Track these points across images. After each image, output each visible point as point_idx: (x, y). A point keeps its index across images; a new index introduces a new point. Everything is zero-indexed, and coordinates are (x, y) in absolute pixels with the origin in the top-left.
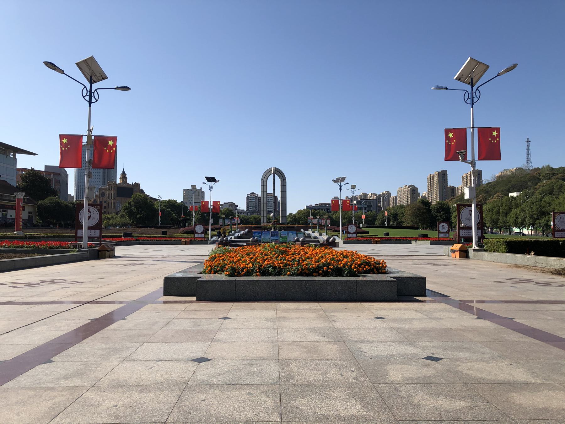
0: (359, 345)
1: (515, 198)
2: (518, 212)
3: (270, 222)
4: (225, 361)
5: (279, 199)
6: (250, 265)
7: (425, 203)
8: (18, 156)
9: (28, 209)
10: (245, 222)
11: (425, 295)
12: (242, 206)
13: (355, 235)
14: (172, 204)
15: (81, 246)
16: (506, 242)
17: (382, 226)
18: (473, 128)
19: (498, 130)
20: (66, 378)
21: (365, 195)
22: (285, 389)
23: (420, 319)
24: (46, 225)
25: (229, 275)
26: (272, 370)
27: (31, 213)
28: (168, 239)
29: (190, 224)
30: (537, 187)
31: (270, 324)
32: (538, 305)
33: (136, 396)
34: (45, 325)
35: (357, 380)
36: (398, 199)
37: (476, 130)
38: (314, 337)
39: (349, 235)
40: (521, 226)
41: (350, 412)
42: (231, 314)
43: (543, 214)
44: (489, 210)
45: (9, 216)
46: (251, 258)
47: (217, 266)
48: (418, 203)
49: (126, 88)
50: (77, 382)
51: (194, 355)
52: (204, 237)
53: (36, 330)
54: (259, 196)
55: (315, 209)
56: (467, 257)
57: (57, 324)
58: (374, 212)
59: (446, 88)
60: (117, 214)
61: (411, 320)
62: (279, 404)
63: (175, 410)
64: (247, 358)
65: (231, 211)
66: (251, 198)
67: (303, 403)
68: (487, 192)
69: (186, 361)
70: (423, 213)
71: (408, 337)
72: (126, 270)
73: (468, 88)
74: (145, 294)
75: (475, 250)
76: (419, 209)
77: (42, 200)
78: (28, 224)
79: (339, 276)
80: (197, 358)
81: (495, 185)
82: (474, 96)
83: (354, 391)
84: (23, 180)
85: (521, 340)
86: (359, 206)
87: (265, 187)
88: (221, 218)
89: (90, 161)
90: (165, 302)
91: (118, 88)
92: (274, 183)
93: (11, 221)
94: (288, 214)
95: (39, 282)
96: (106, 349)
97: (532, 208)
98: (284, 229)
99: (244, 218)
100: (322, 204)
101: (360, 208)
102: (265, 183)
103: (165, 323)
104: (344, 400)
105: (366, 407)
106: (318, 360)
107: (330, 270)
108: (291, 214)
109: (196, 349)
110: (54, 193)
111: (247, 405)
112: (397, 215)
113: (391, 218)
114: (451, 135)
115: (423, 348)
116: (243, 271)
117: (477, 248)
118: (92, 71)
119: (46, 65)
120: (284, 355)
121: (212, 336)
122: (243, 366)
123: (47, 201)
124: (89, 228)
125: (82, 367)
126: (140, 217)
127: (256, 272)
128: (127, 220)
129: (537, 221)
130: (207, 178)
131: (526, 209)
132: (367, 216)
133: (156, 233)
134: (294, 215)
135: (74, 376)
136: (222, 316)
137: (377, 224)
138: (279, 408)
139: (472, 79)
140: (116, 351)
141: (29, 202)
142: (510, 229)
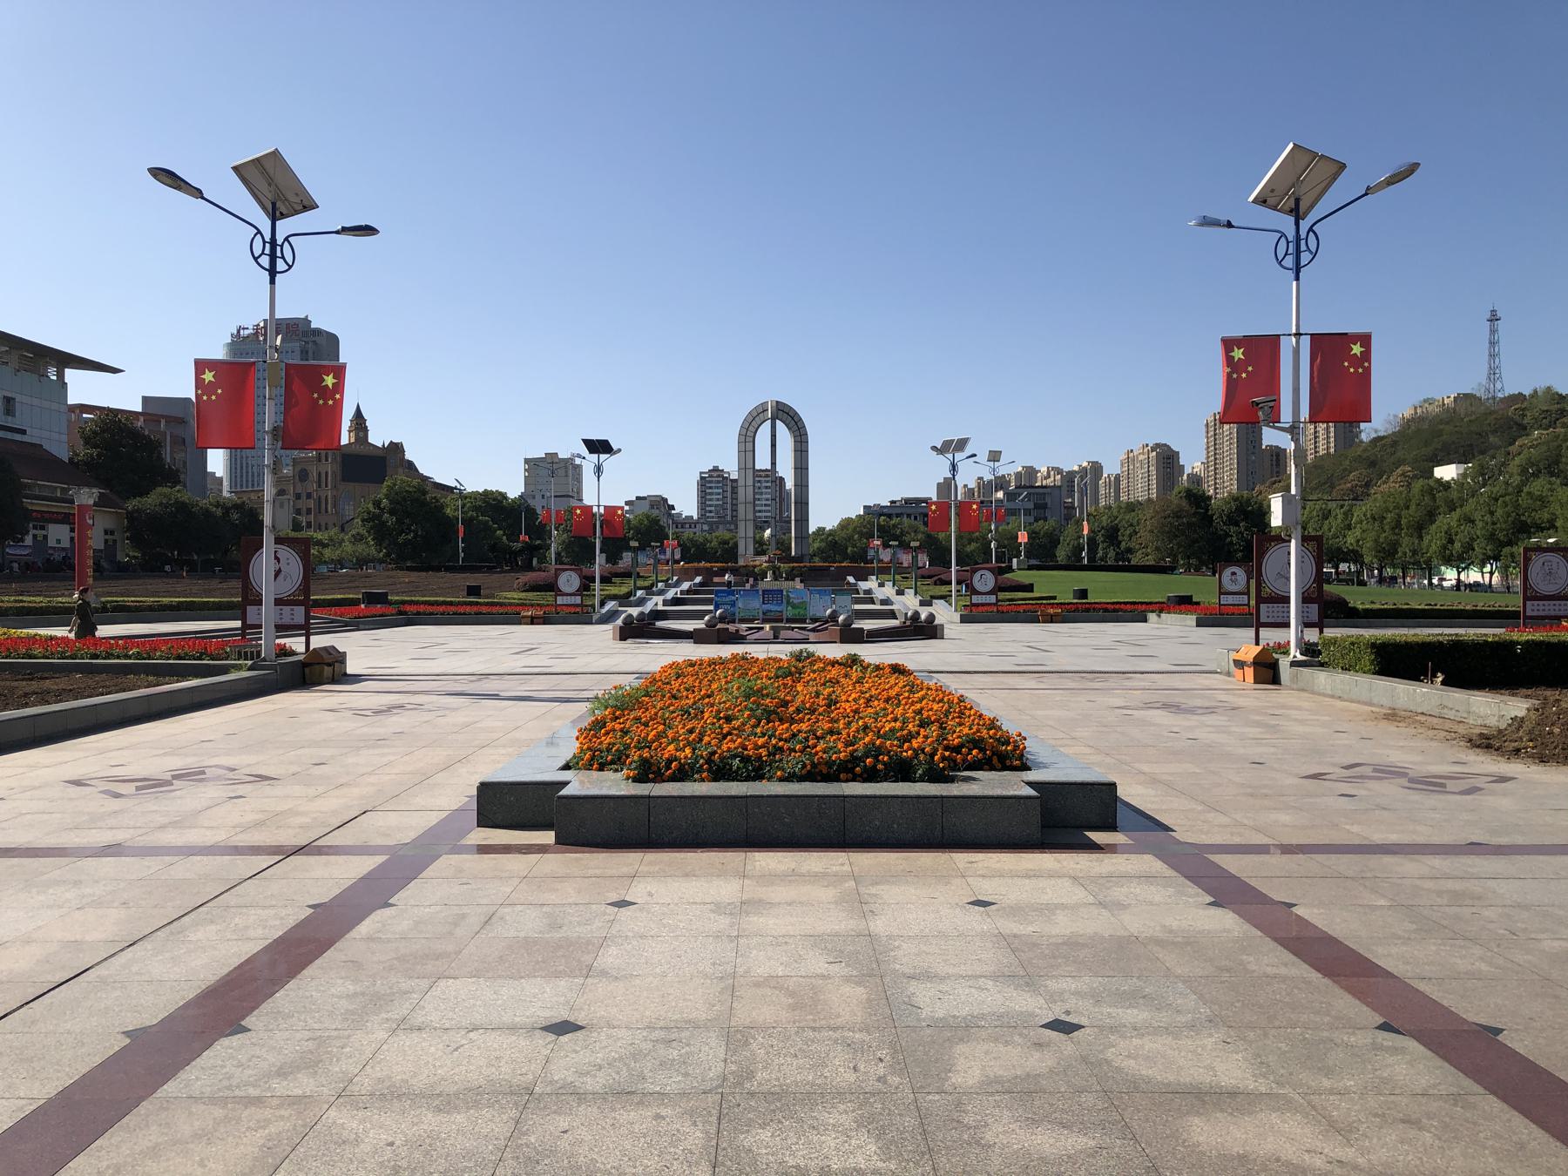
0: (913, 987)
1: (1444, 485)
3: (763, 553)
4: (613, 1032)
5: (790, 484)
7: (1196, 497)
8: (71, 375)
10: (694, 552)
11: (1111, 827)
12: (686, 505)
13: (992, 599)
14: (492, 503)
15: (259, 653)
16: (1373, 645)
17: (1074, 565)
18: (1298, 335)
19: (1365, 340)
20: (282, 1072)
21: (1031, 472)
22: (733, 1103)
23: (1074, 908)
24: (151, 567)
25: (637, 780)
26: (711, 1056)
27: (112, 533)
28: (484, 609)
29: (543, 559)
30: (1513, 449)
31: (723, 922)
35: (885, 1082)
36: (1123, 484)
37: (1306, 342)
38: (817, 963)
39: (976, 599)
40: (1460, 561)
41: (851, 1162)
42: (637, 892)
43: (1524, 528)
45: (52, 543)
46: (691, 731)
47: (609, 750)
48: (1174, 497)
49: (368, 230)
50: (303, 1084)
51: (547, 1014)
52: (582, 605)
53: (193, 937)
54: (734, 476)
55: (890, 516)
56: (1275, 680)
58: (1052, 522)
59: (1229, 225)
62: (714, 1143)
64: (662, 1024)
65: (655, 521)
66: (711, 482)
67: (761, 1140)
68: (1373, 464)
70: (1189, 525)
71: (1026, 962)
73: (1286, 223)
74: (433, 819)
75: (1294, 664)
76: (1177, 515)
77: (141, 495)
78: (109, 568)
80: (554, 1021)
81: (1394, 444)
82: (1303, 247)
83: (872, 1111)
84: (88, 441)
85: (1283, 971)
86: (1011, 505)
88: (629, 549)
90: (484, 849)
91: (345, 230)
92: (773, 445)
93: (58, 557)
94: (812, 529)
95: (168, 776)
96: (355, 994)
97: (1492, 513)
99: (691, 540)
100: (908, 501)
101: (1013, 512)
102: (749, 446)
103: (483, 919)
104: (846, 1133)
105: (885, 1153)
106: (814, 1029)
107: (880, 766)
108: (821, 530)
109: (547, 998)
110: (172, 477)
111: (650, 1145)
113: (1100, 538)
115: (1053, 998)
116: (668, 768)
117: (1300, 657)
118: (275, 187)
119: (155, 176)
120: (744, 1014)
121: (587, 959)
122: (650, 1046)
123: (152, 501)
124: (278, 602)
126: (407, 542)
127: (700, 771)
128: (370, 548)
129: (1506, 550)
130: (585, 441)
131: (1477, 516)
132: (1032, 535)
133: (447, 586)
134: (832, 533)
136: (614, 897)
137: (1061, 554)
138: (713, 1151)
139: (1297, 201)
140: (377, 1001)
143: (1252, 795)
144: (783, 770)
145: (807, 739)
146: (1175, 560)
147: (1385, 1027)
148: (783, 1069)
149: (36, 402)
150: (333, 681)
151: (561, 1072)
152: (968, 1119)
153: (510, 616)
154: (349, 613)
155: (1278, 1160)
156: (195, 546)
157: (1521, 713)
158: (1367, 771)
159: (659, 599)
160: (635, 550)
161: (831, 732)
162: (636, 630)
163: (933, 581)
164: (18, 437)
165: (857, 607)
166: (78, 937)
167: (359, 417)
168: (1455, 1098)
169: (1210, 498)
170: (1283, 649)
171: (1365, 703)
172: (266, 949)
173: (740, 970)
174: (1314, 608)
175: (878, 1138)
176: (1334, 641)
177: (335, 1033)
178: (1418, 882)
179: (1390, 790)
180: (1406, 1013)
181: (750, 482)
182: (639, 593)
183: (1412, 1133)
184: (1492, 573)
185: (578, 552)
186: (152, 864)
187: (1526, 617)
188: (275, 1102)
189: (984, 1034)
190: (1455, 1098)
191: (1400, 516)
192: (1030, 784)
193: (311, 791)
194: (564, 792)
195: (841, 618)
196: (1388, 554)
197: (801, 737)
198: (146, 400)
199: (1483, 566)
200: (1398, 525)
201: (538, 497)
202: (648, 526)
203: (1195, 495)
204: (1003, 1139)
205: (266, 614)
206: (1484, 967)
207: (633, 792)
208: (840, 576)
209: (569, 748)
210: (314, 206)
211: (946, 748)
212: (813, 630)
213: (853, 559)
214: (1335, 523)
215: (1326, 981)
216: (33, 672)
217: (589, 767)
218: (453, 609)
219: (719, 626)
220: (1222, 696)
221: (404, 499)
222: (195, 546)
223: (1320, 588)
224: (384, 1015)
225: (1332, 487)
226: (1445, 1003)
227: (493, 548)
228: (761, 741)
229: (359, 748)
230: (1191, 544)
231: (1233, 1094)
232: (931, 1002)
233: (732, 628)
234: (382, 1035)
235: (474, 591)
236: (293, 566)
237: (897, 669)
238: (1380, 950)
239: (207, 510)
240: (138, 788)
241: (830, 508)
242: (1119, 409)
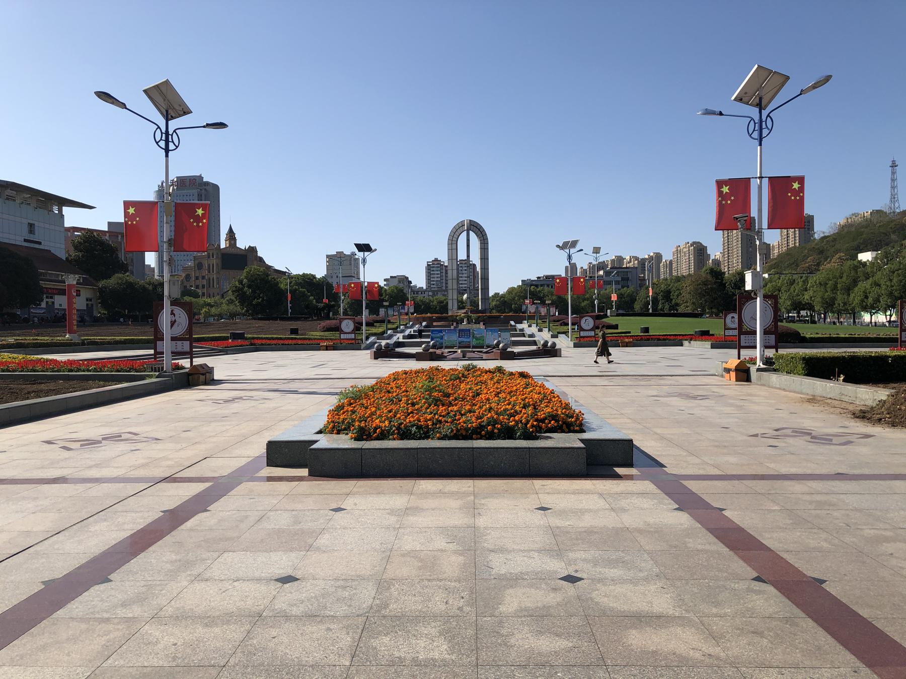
0: (492, 556)
1: (864, 264)
2: (868, 286)
3: (463, 308)
6: (387, 422)
7: (716, 273)
8: (66, 210)
9: (86, 293)
10: (422, 308)
11: (630, 465)
12: (419, 280)
14: (308, 281)
15: (163, 368)
16: (804, 359)
18: (761, 177)
19: (801, 180)
20: (124, 605)
21: (620, 259)
24: (113, 319)
25: (356, 439)
26: (366, 595)
27: (91, 300)
28: (300, 342)
29: (336, 313)
31: (393, 519)
32: (778, 483)
33: (200, 631)
34: (105, 520)
36: (674, 265)
37: (766, 182)
38: (440, 543)
39: (582, 334)
40: (872, 308)
41: (431, 655)
42: (348, 504)
44: (820, 284)
45: (57, 306)
46: (390, 411)
47: (343, 422)
48: (703, 272)
49: (221, 125)
50: (136, 611)
51: (281, 571)
52: (355, 339)
53: (92, 529)
55: (537, 286)
56: (748, 379)
57: (120, 520)
58: (631, 289)
59: (721, 114)
60: (223, 297)
61: (581, 512)
63: (239, 650)
64: (343, 577)
65: (401, 290)
66: (434, 267)
68: (821, 252)
69: (269, 580)
72: (226, 412)
73: (754, 112)
74: (243, 462)
75: (759, 370)
76: (705, 283)
78: (87, 319)
79: (509, 438)
80: (283, 576)
81: (835, 240)
82: (764, 126)
84: (76, 247)
85: (708, 547)
87: (454, 251)
88: (383, 306)
89: (169, 240)
90: (270, 479)
91: (208, 125)
92: (468, 246)
93: (60, 314)
94: (491, 294)
95: (100, 438)
96: (176, 561)
97: (891, 280)
98: (483, 321)
99: (422, 301)
100: (547, 277)
101: (610, 283)
102: (454, 246)
103: (257, 518)
105: (451, 651)
106: (429, 580)
108: (497, 295)
109: (282, 563)
110: (124, 268)
111: (320, 645)
112: (669, 292)
113: (660, 297)
114: (725, 189)
115: (569, 563)
117: (762, 366)
118: (168, 101)
119: (99, 96)
121: (310, 541)
123: (113, 281)
124: (173, 339)
125: (144, 589)
128: (237, 308)
131: (882, 282)
132: (620, 296)
133: (280, 329)
134: (503, 296)
135: (134, 602)
136: (335, 506)
137: (637, 307)
138: (354, 649)
139: (761, 99)
140: (187, 564)
141: (85, 283)
142: (854, 315)
143: (716, 446)
144: (440, 433)
145: (455, 415)
146: (703, 310)
147: (757, 579)
148: (405, 602)
149: (47, 226)
150: (206, 384)
151: (280, 604)
152: (504, 631)
153: (313, 346)
154: (221, 345)
155: (674, 654)
156: (133, 306)
157: (884, 398)
158: (789, 432)
159: (400, 336)
160: (386, 307)
161: (470, 411)
162: (381, 354)
163: (558, 324)
164: (37, 246)
165: (513, 339)
166: (29, 529)
167: (231, 231)
168: (787, 620)
169: (724, 273)
170: (753, 361)
171: (798, 393)
172: (132, 536)
173: (395, 547)
174: (772, 338)
175: (450, 641)
176: (782, 357)
177: (158, 583)
178: (800, 496)
179: (799, 443)
180: (776, 573)
181: (455, 267)
182: (389, 332)
183: (757, 639)
184: (891, 316)
185: (355, 309)
186: (80, 487)
187: (901, 342)
188: (116, 621)
189: (525, 582)
190: (787, 620)
191: (836, 283)
192: (582, 441)
193: (179, 446)
194: (314, 446)
195: (501, 345)
196: (829, 305)
197: (451, 414)
198: (110, 224)
199: (885, 312)
200: (835, 288)
201: (335, 277)
202: (397, 293)
203: (716, 272)
204: (521, 642)
205: (166, 346)
206: (825, 545)
207: (353, 446)
208: (506, 321)
209: (322, 421)
210: (190, 112)
211: (537, 420)
212: (486, 352)
213: (516, 311)
214: (798, 287)
215: (731, 553)
216: (35, 380)
217: (331, 432)
218: (282, 342)
219: (431, 350)
220: (715, 389)
221: (256, 279)
222: (133, 306)
223: (776, 326)
224: (189, 573)
225: (797, 266)
226: (796, 565)
227: (307, 307)
228: (429, 417)
229: (211, 422)
230: (703, 301)
231: (659, 617)
232: (500, 565)
233: (439, 352)
234: (185, 583)
235: (294, 331)
236: (182, 317)
237: (523, 375)
238: (767, 535)
239: (144, 287)
240: (82, 445)
241: (501, 282)
242: (662, 224)
